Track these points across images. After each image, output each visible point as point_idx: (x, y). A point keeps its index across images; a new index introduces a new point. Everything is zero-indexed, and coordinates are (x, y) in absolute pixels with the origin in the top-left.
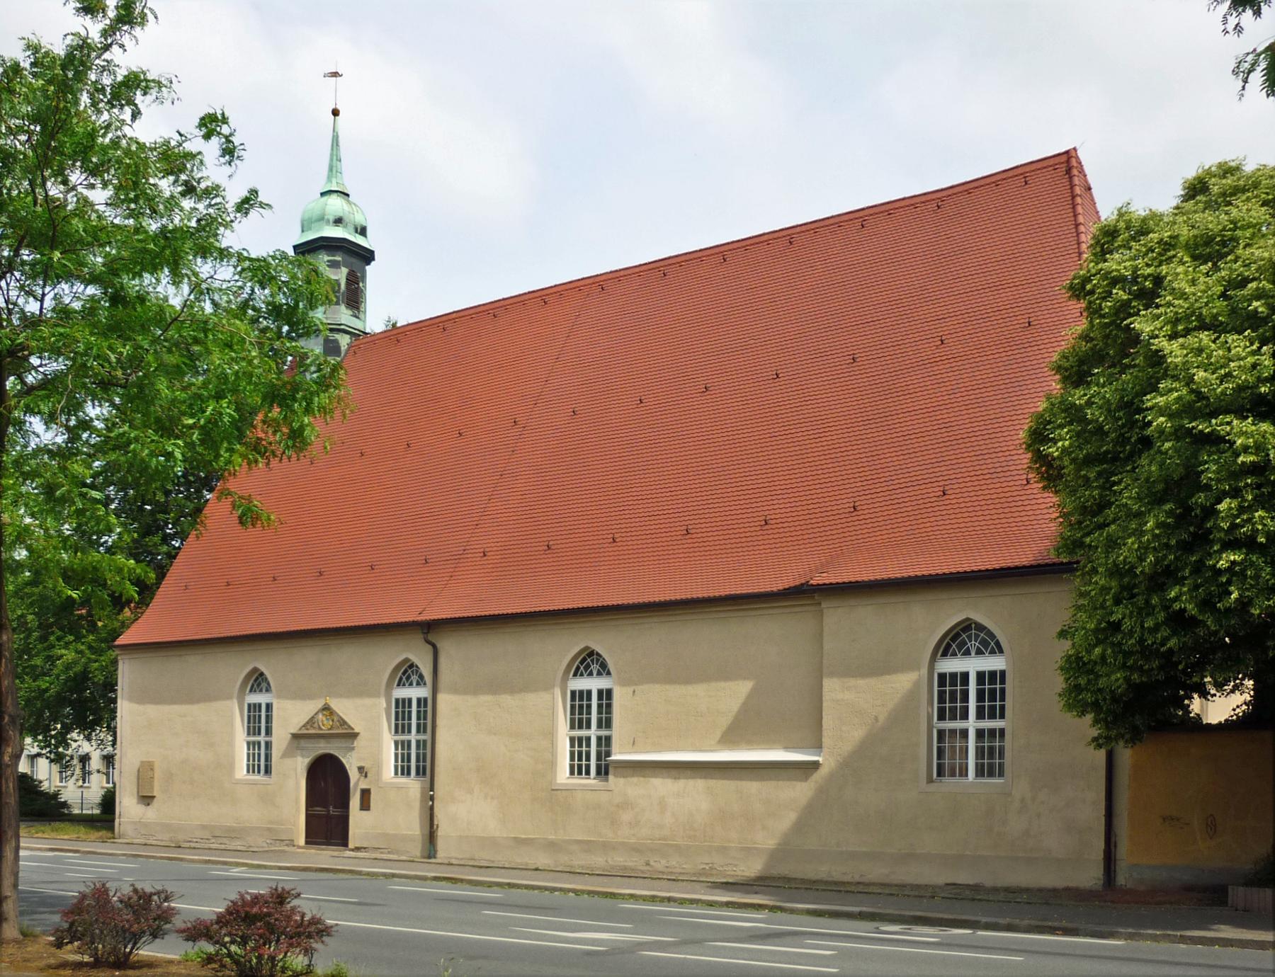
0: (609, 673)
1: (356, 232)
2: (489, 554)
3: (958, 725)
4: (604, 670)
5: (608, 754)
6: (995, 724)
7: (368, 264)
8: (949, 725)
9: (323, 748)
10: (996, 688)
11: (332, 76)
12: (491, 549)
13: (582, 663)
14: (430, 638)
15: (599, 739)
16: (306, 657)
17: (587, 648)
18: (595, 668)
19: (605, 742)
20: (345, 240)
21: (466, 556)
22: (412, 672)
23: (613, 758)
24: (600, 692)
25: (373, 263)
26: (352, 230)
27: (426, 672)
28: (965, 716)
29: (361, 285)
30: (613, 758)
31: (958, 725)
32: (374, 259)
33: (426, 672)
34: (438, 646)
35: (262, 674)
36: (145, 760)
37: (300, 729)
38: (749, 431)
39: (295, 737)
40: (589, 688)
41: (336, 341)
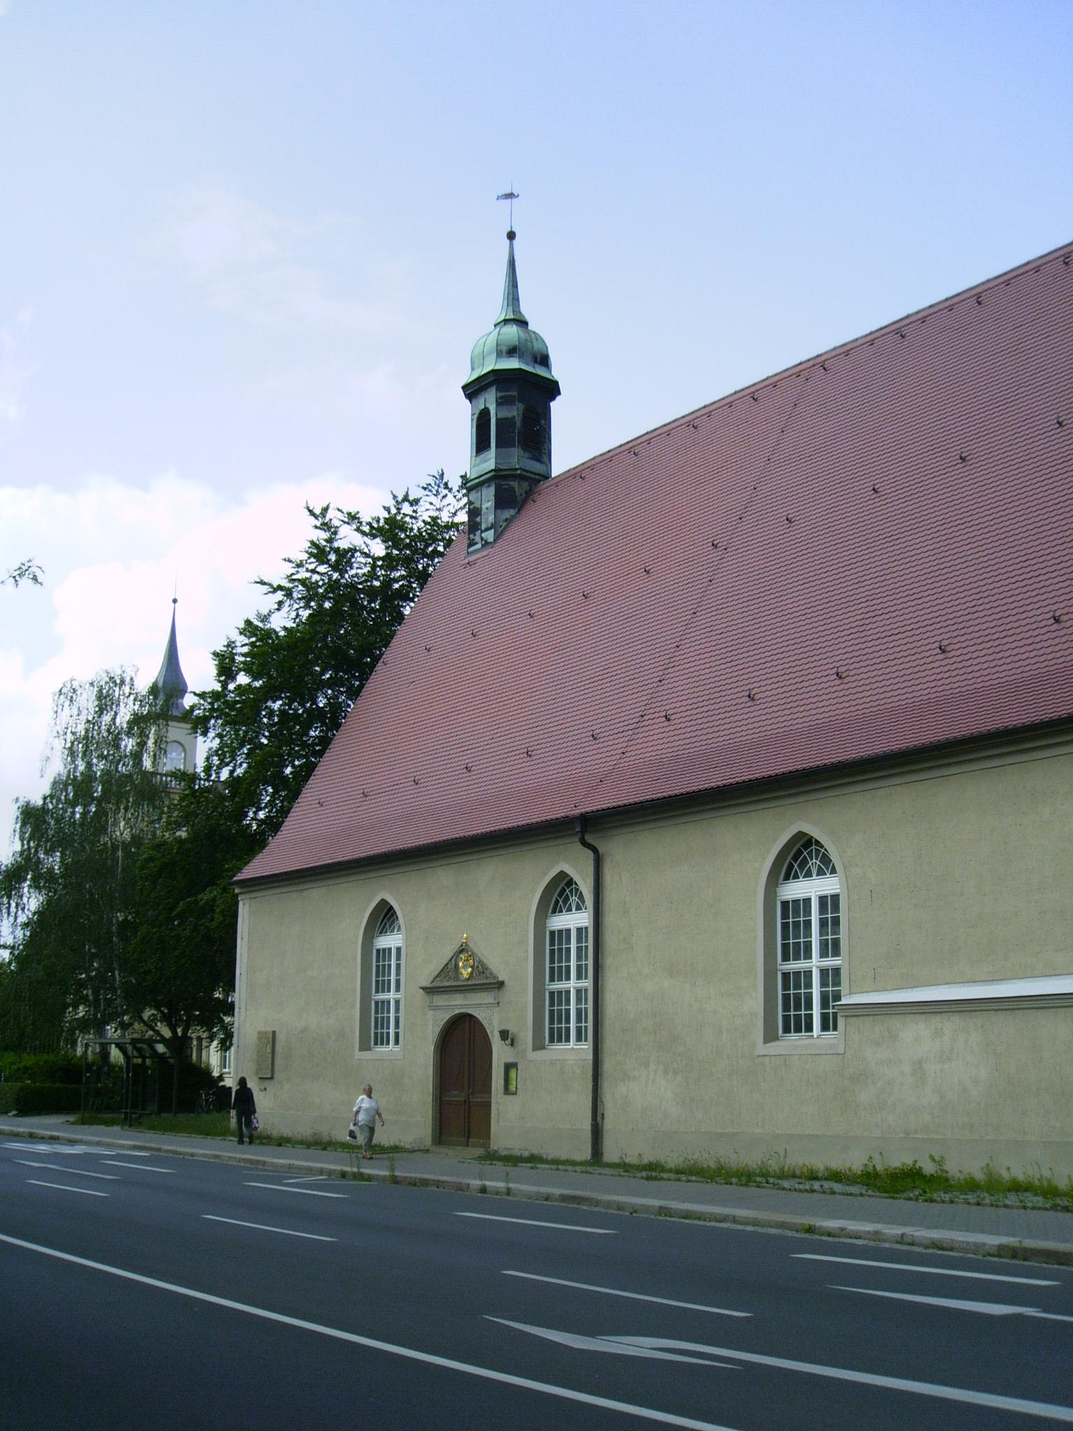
0: (834, 871)
1: (535, 361)
2: (673, 717)
3: (800, 965)
4: (827, 866)
5: (837, 997)
6: (381, 997)
7: (553, 399)
8: (793, 966)
9: (458, 1004)
10: (794, 990)
11: (506, 198)
12: (674, 711)
13: (795, 858)
14: (589, 838)
15: (824, 972)
16: (443, 876)
17: (800, 835)
18: (814, 863)
19: (831, 976)
20: (520, 369)
21: (644, 723)
22: (571, 891)
23: (844, 1001)
24: (823, 900)
25: (558, 398)
26: (529, 359)
27: (586, 886)
28: (808, 956)
29: (543, 422)
30: (844, 1001)
31: (800, 965)
32: (559, 393)
33: (586, 886)
34: (601, 850)
35: (571, 882)
36: (263, 1030)
37: (433, 982)
38: (996, 643)
39: (429, 991)
40: (805, 896)
41: (512, 489)
